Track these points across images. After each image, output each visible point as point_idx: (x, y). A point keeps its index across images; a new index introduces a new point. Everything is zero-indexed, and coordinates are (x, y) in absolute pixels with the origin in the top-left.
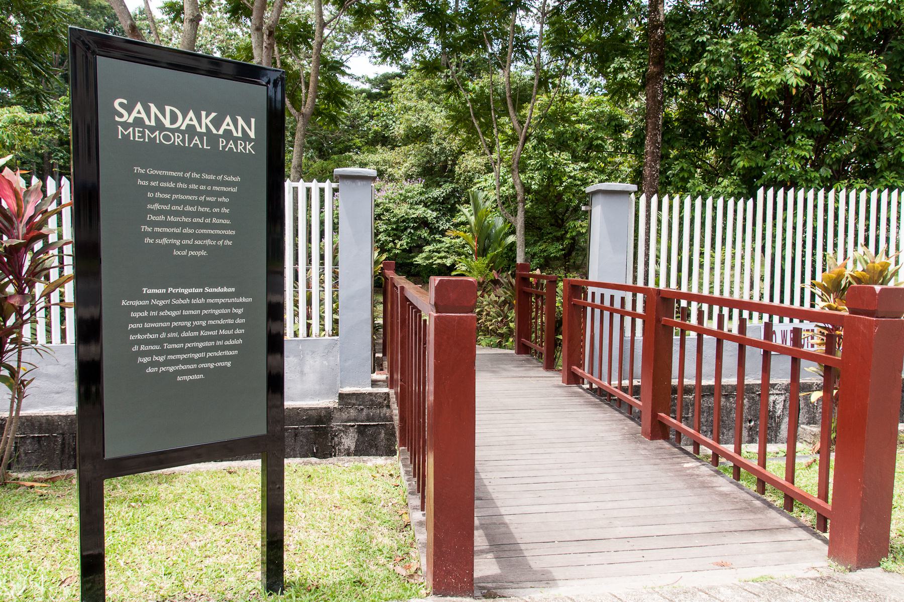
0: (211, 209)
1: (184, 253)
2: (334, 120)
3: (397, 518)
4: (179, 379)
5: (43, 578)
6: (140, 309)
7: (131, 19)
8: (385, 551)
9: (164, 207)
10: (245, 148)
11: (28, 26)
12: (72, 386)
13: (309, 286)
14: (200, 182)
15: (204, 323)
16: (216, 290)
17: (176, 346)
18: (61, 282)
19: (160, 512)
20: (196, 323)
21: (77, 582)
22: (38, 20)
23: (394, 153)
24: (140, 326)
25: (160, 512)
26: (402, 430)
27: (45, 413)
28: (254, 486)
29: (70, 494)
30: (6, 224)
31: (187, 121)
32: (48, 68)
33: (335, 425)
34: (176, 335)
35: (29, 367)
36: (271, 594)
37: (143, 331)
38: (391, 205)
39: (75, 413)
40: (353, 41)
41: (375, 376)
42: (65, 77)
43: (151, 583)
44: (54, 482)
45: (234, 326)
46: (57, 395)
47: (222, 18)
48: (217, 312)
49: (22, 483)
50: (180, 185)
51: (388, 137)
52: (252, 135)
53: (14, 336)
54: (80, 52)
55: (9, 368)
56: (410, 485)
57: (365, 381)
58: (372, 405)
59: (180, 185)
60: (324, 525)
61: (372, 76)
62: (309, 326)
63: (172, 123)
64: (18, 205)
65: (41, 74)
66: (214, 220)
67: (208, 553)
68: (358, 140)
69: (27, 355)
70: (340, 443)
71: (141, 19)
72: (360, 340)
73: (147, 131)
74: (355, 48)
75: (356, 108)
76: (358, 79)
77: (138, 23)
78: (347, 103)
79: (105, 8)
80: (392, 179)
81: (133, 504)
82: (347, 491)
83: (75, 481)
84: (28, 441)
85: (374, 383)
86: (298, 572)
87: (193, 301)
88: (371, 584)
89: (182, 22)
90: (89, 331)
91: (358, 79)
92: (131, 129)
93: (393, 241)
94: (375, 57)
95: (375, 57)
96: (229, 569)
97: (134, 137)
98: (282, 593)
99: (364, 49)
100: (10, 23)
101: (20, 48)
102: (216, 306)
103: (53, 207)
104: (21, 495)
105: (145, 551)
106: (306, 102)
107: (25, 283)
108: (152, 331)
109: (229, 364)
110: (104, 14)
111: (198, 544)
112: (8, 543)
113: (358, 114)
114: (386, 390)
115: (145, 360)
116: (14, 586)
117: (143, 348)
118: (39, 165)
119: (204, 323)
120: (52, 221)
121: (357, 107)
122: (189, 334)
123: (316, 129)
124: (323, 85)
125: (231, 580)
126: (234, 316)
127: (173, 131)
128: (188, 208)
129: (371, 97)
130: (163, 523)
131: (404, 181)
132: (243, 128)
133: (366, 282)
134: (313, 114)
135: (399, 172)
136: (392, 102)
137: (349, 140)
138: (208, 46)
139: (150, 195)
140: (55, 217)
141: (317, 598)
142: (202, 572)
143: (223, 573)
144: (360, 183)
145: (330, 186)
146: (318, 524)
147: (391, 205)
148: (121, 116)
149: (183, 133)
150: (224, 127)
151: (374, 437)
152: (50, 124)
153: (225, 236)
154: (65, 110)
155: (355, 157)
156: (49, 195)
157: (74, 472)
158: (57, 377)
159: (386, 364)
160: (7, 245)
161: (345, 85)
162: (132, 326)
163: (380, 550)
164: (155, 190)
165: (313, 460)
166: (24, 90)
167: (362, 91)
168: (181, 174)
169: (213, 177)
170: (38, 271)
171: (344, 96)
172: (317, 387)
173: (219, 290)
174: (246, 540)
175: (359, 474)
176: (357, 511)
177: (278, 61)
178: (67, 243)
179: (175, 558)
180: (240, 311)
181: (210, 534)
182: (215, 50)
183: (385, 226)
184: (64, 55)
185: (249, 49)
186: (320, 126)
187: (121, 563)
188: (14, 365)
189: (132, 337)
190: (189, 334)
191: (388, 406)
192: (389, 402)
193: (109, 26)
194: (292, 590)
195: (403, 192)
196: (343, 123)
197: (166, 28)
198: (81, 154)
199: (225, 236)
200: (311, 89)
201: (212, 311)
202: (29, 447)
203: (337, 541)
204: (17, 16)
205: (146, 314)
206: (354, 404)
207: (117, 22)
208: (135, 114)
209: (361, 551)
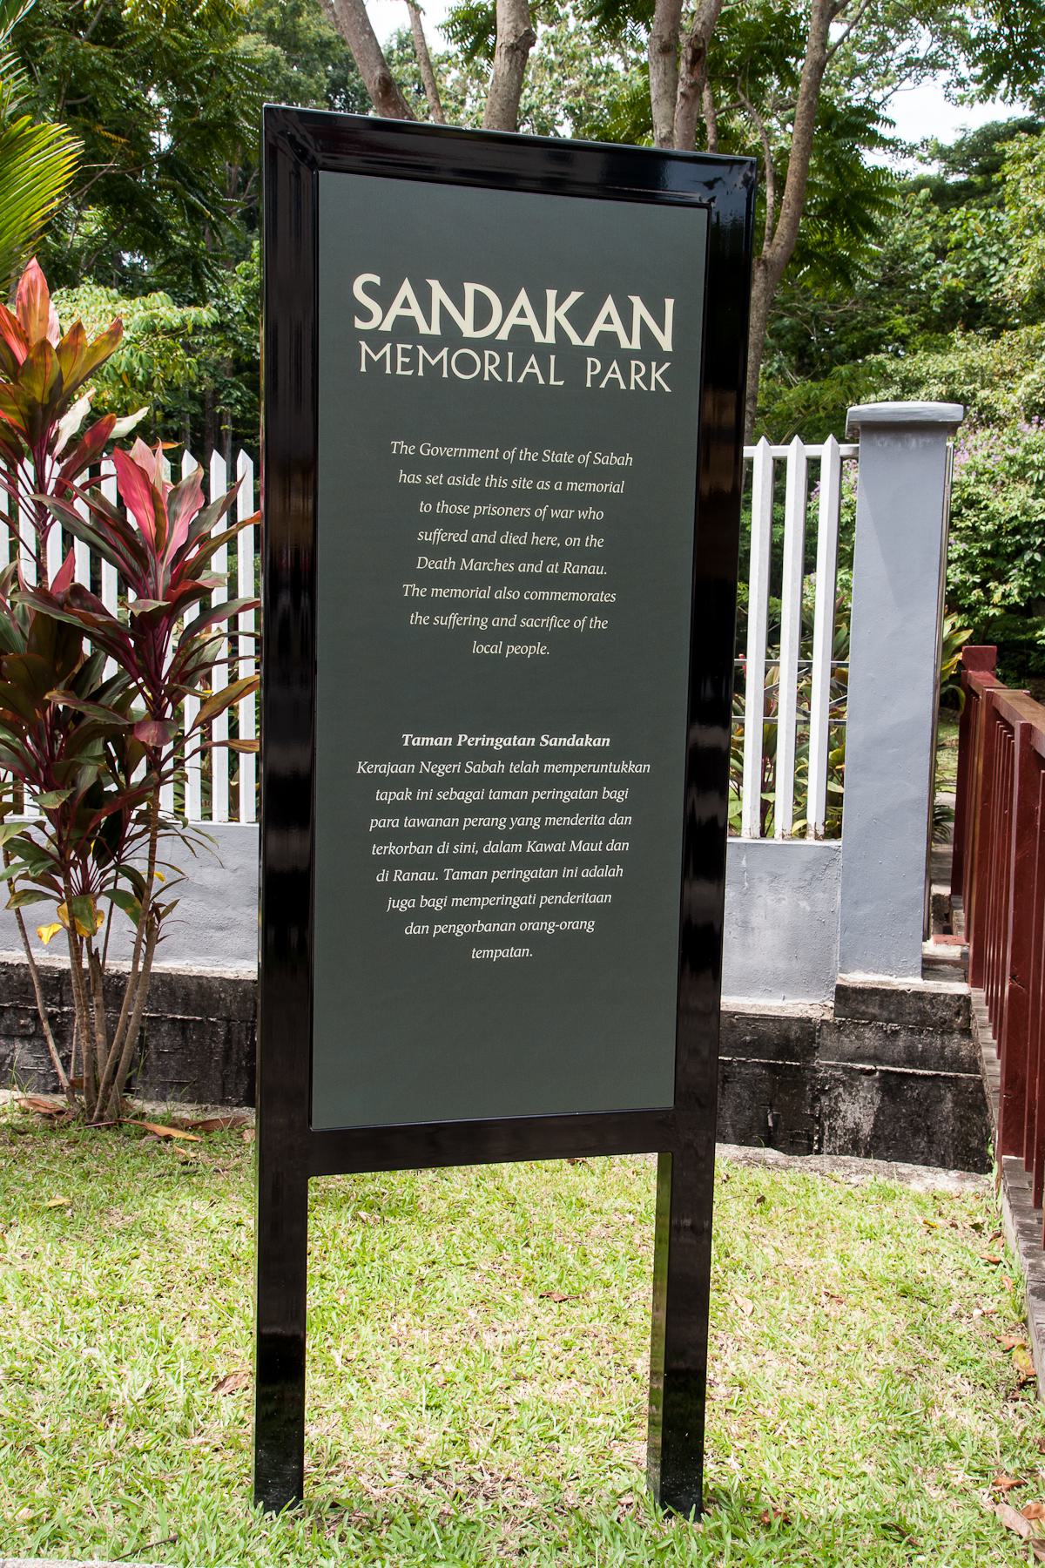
0: (561, 541)
1: (496, 650)
2: (842, 270)
3: (997, 1355)
4: (476, 954)
5: (183, 1367)
6: (395, 783)
7: (384, 65)
8: (967, 1451)
9: (454, 537)
10: (646, 379)
11: (182, 108)
12: (251, 916)
13: (770, 708)
14: (537, 471)
15: (535, 824)
16: (565, 742)
17: (470, 875)
18: (234, 693)
19: (418, 1242)
20: (519, 822)
21: (248, 1393)
22: (201, 91)
23: (997, 347)
24: (394, 823)
25: (418, 1242)
26: (1012, 1110)
27: (196, 970)
28: (629, 1206)
29: (238, 1169)
30: (134, 564)
31: (513, 319)
32: (215, 200)
33: (823, 1064)
34: (470, 848)
35: (172, 876)
36: (669, 1515)
37: (400, 836)
38: (981, 489)
39: (254, 977)
40: (904, 47)
41: (933, 948)
42: (250, 219)
43: (399, 1424)
44: (208, 1132)
45: (605, 834)
46: (219, 934)
47: (579, 31)
48: (567, 797)
49: (151, 1126)
50: (492, 481)
51: (985, 304)
52: (666, 342)
53: (144, 807)
54: (286, 162)
55: (133, 875)
56: (1033, 1267)
57: (912, 959)
58: (923, 1023)
59: (492, 481)
60: (802, 1341)
61: (949, 140)
62: (766, 808)
63: (476, 329)
64: (157, 524)
65: (203, 214)
66: (569, 568)
67: (521, 1368)
68: (900, 320)
69: (168, 848)
70: (834, 1112)
71: (402, 61)
72: (900, 856)
73: (422, 350)
74: (909, 63)
75: (900, 230)
76: (910, 151)
77: (395, 70)
78: (878, 218)
79: (328, 44)
80: (988, 418)
81: (363, 1214)
82: (861, 1253)
83: (250, 1136)
84: (165, 1028)
85: (930, 967)
86: (736, 1466)
87: (513, 769)
88: (932, 1542)
89: (490, 55)
90: (286, 803)
91: (910, 151)
92: (387, 348)
93: (982, 585)
94: (961, 83)
95: (961, 83)
96: (571, 1423)
97: (394, 367)
98: (698, 1519)
99: (932, 63)
100: (148, 105)
101: (166, 159)
102: (565, 782)
103: (219, 528)
104: (147, 1155)
105: (387, 1338)
106: (773, 229)
107: (164, 696)
108: (420, 836)
109: (589, 927)
110: (325, 59)
111: (501, 1340)
112: (123, 1270)
113: (904, 248)
114: (961, 988)
115: (403, 905)
116: (129, 1374)
117: (398, 876)
118: (192, 426)
119: (535, 824)
120: (219, 561)
121: (904, 228)
122: (503, 848)
123: (793, 298)
124: (819, 179)
125: (574, 1452)
126: (607, 808)
127: (479, 345)
128: (510, 539)
129: (944, 196)
130: (425, 1272)
131: (1022, 423)
132: (643, 323)
133: (923, 701)
134: (792, 260)
135: (1007, 400)
136: (1001, 205)
137: (879, 320)
138: (545, 109)
139: (424, 508)
140: (224, 548)
141: (785, 1553)
142: (506, 1418)
143: (555, 1431)
144: (914, 442)
145: (835, 451)
146: (785, 1338)
147: (981, 489)
148: (367, 315)
149: (502, 348)
150: (599, 325)
151: (926, 1107)
152: (219, 327)
153: (591, 608)
154: (246, 291)
155: (891, 366)
156: (213, 499)
157: (249, 1115)
158: (220, 894)
159: (960, 916)
160: (137, 612)
161: (879, 172)
162: (376, 823)
163: (952, 1445)
164: (435, 494)
165: (771, 1154)
166: (171, 253)
167: (921, 184)
168: (493, 454)
169: (567, 458)
170: (192, 670)
171: (875, 203)
172: (782, 965)
173: (574, 742)
174: (609, 1348)
175: (888, 1210)
176: (890, 1320)
177: (710, 129)
178: (245, 608)
179: (450, 1367)
180: (620, 796)
181: (528, 1318)
182: (560, 117)
183: (964, 546)
184: (247, 167)
185: (640, 104)
186: (806, 290)
187: (337, 1356)
188: (141, 866)
189: (376, 850)
190: (503, 848)
191: (966, 1032)
192: (969, 1020)
193: (337, 85)
194: (723, 1514)
195: (1018, 452)
196: (866, 276)
197: (455, 74)
198: (274, 397)
199: (591, 608)
200: (788, 195)
201: (554, 794)
202: (165, 1040)
203: (837, 1395)
204: (162, 89)
205: (408, 795)
206: (874, 1018)
207: (352, 75)
208: (396, 310)
209: (900, 1436)
